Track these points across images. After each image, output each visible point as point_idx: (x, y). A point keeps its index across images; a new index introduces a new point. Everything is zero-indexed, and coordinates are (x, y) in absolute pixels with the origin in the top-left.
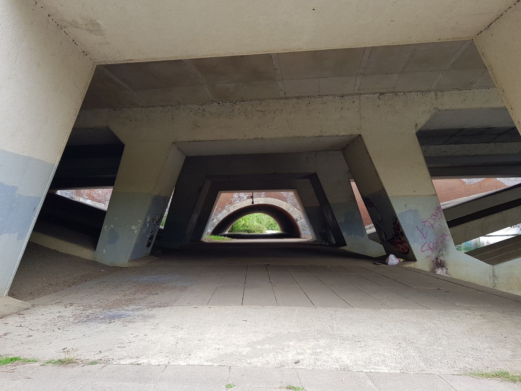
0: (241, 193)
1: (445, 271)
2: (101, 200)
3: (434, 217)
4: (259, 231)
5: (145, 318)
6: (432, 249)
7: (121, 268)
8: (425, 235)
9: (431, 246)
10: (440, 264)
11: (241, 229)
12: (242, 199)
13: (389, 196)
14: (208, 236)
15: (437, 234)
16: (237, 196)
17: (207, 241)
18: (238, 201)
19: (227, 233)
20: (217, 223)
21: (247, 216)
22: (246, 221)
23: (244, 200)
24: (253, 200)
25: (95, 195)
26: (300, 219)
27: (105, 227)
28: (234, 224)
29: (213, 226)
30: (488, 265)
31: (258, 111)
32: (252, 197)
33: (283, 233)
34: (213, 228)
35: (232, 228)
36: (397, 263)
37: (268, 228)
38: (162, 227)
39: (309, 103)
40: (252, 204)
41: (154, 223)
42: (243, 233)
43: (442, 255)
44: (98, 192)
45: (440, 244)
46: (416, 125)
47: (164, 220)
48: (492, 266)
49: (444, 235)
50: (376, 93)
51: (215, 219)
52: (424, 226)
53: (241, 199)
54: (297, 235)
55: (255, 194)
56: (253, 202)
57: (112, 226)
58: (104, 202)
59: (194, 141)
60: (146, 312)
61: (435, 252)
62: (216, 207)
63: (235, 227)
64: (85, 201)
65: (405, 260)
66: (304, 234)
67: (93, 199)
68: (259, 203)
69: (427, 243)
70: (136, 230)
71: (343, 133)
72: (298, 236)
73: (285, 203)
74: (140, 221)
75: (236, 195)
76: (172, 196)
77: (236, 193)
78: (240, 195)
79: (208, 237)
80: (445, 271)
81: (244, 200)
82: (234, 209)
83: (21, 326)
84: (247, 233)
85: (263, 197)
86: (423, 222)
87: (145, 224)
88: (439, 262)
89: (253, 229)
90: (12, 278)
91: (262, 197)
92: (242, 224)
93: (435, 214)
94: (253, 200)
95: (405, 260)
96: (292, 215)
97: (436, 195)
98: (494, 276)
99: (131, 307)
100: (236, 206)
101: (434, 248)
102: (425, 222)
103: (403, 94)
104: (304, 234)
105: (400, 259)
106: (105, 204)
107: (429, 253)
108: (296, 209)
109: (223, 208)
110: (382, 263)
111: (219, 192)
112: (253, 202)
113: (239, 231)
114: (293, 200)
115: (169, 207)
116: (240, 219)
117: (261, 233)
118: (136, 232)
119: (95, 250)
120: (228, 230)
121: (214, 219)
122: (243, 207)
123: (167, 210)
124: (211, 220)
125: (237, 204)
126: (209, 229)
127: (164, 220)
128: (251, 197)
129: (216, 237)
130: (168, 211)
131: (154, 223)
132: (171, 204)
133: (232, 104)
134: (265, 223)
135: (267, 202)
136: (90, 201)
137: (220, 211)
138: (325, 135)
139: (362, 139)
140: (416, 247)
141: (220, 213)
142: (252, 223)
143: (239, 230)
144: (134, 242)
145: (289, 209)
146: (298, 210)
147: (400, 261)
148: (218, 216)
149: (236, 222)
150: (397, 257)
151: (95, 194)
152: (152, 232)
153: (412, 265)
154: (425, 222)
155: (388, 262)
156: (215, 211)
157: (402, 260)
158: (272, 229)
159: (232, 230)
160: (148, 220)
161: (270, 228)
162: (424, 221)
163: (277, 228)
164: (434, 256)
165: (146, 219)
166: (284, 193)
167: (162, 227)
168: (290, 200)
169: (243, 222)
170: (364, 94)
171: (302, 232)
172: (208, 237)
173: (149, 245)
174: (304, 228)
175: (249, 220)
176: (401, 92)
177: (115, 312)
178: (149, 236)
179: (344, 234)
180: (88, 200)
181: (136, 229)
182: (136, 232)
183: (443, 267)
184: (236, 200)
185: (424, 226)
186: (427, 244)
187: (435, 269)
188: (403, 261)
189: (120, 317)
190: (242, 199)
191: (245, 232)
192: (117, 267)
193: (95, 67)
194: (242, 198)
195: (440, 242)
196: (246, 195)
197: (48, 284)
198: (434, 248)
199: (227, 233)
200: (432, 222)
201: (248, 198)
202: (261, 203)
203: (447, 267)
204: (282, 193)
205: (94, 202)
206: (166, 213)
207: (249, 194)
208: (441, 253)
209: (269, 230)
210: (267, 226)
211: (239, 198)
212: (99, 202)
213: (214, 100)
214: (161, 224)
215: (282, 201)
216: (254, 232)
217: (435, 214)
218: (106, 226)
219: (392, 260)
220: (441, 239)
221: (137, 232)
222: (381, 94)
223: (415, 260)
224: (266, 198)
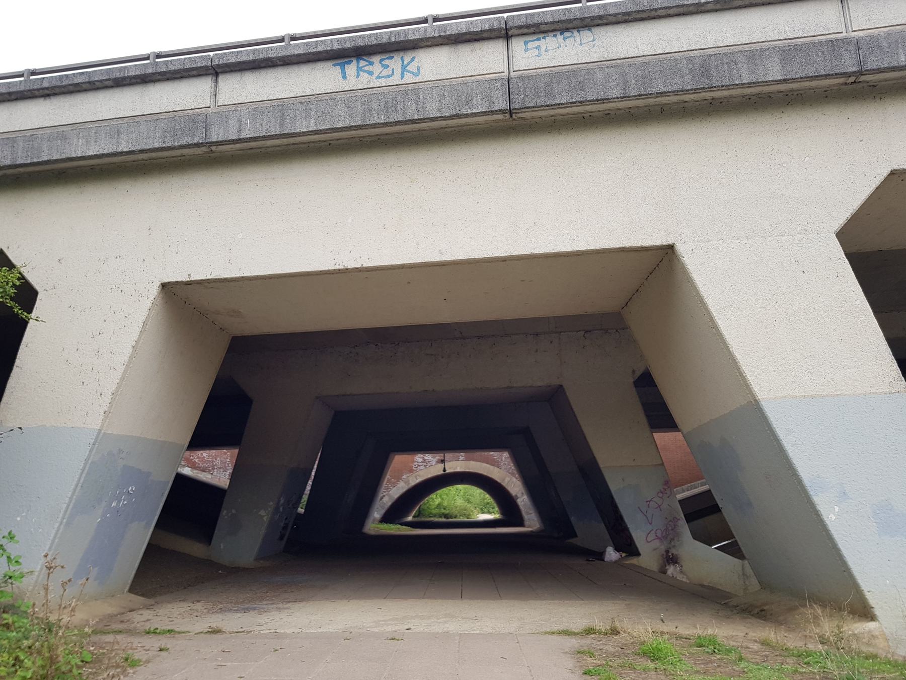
0: (427, 455)
1: (679, 568)
2: (207, 467)
3: (660, 495)
5: (279, 609)
6: (660, 538)
7: (245, 570)
8: (650, 521)
9: (659, 535)
10: (671, 559)
11: (434, 512)
12: (429, 464)
13: (601, 466)
14: (374, 525)
15: (666, 518)
16: (421, 460)
17: (372, 533)
18: (422, 467)
19: (410, 518)
20: (390, 504)
21: (445, 489)
22: (442, 499)
24: (444, 466)
25: (197, 461)
27: (224, 513)
28: (421, 503)
30: (736, 560)
31: (427, 354)
32: (443, 461)
33: (405, 518)
34: (383, 512)
36: (617, 559)
37: (482, 509)
38: (301, 510)
39: (494, 344)
40: (443, 472)
41: (291, 505)
42: (436, 519)
43: (674, 546)
44: (202, 454)
45: (671, 532)
46: (634, 371)
47: (305, 498)
48: (741, 561)
49: (675, 520)
50: (580, 331)
51: (386, 497)
52: (649, 507)
54: (520, 522)
55: (448, 456)
56: (444, 468)
57: (234, 511)
58: (210, 471)
59: (343, 395)
60: (280, 606)
61: (665, 542)
62: (388, 477)
64: (182, 470)
65: (627, 554)
67: (193, 466)
69: (653, 530)
70: (266, 516)
71: (539, 384)
72: (520, 522)
73: (496, 469)
74: (271, 503)
75: (419, 458)
76: (318, 459)
77: (419, 455)
78: (426, 458)
79: (374, 525)
80: (679, 568)
81: (432, 465)
82: (417, 479)
83: (157, 615)
84: (444, 520)
86: (647, 501)
87: (277, 509)
88: (671, 556)
89: (456, 512)
90: (134, 572)
91: (461, 460)
92: (437, 503)
93: (662, 490)
94: (444, 466)
95: (627, 554)
96: (509, 489)
97: (663, 464)
98: (744, 574)
99: (265, 602)
101: (663, 537)
102: (650, 501)
103: (615, 331)
105: (621, 553)
106: (212, 474)
107: (657, 543)
109: (399, 478)
110: (598, 559)
111: (391, 455)
112: (444, 468)
113: (431, 515)
114: (509, 465)
115: (313, 477)
116: (433, 496)
118: (265, 518)
119: (210, 544)
121: (384, 496)
122: (430, 476)
123: (310, 482)
124: (379, 498)
125: (421, 473)
126: (377, 514)
127: (305, 498)
129: (392, 526)
130: (311, 483)
131: (291, 505)
132: (316, 472)
133: (393, 345)
134: (478, 501)
136: (190, 469)
137: (394, 483)
138: (515, 385)
139: (564, 390)
140: (639, 536)
141: (394, 487)
142: (453, 502)
143: (431, 513)
144: (263, 532)
145: (504, 480)
147: (621, 556)
148: (390, 492)
150: (617, 549)
151: (198, 458)
152: (286, 519)
153: (634, 561)
154: (650, 501)
155: (604, 558)
156: (385, 483)
157: (624, 555)
158: (489, 513)
159: (419, 514)
160: (282, 501)
162: (648, 500)
164: (663, 548)
165: (279, 501)
166: (495, 455)
167: (301, 510)
168: (505, 464)
169: (438, 501)
170: (564, 332)
171: (526, 517)
172: (374, 525)
173: (281, 538)
175: (448, 496)
176: (612, 329)
177: (247, 606)
178: (282, 524)
179: (573, 519)
180: (187, 468)
181: (265, 515)
182: (265, 518)
183: (676, 563)
185: (649, 507)
186: (653, 532)
187: (666, 566)
188: (626, 556)
189: (254, 609)
190: (429, 464)
191: (441, 517)
192: (239, 568)
193: (231, 338)
194: (429, 462)
195: (670, 528)
196: (434, 457)
197: (159, 586)
198: (663, 537)
199: (410, 518)
200: (659, 501)
201: (438, 462)
202: (458, 470)
203: (681, 563)
204: (492, 453)
205: (195, 471)
206: (309, 488)
207: (439, 456)
208: (673, 543)
209: (483, 513)
210: (481, 507)
212: (204, 471)
213: (369, 341)
214: (301, 505)
215: (492, 467)
216: (456, 517)
217: (662, 490)
218: (225, 512)
219: (610, 554)
220: (672, 524)
221: (267, 519)
222: (586, 332)
223: (638, 554)
224: (468, 463)
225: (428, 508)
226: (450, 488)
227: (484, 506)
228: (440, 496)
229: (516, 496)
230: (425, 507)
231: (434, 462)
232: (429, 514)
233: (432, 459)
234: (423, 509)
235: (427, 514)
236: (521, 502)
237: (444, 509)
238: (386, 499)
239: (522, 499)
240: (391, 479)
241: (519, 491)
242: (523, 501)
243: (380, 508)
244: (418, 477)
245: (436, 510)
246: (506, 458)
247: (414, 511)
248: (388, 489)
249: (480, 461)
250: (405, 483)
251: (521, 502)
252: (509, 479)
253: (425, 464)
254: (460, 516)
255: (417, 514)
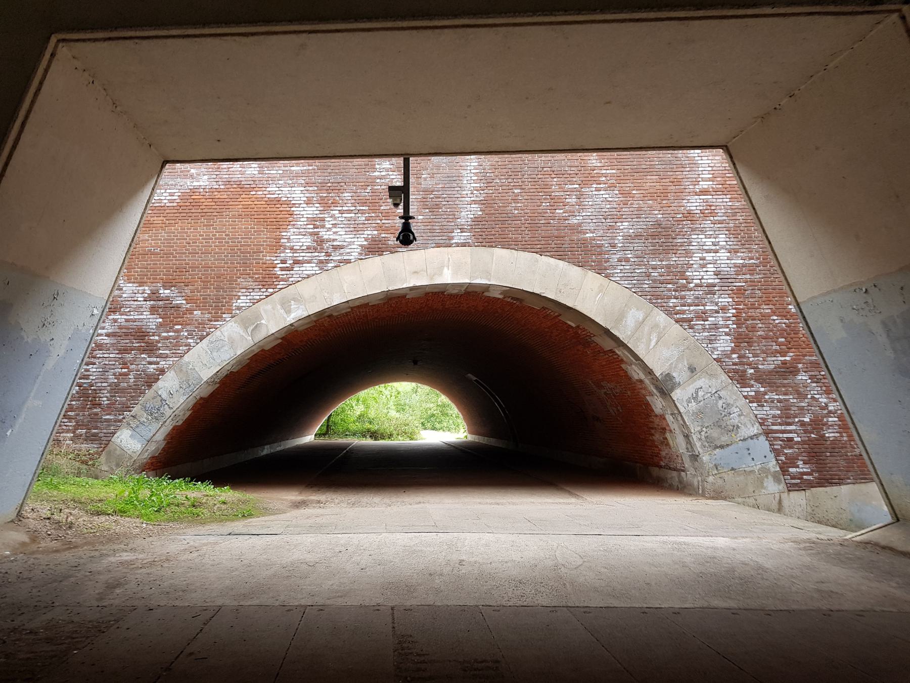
4: (406, 433)
11: (353, 427)
16: (307, 241)
18: (309, 268)
23: (348, 262)
26: (686, 374)
29: (154, 414)
33: (289, 441)
35: (328, 426)
37: (423, 424)
53: (328, 254)
63: (336, 421)
66: (716, 467)
68: (439, 281)
73: (592, 280)
82: (288, 312)
84: (368, 442)
85: (464, 245)
89: (387, 427)
91: (458, 245)
92: (358, 413)
100: (298, 299)
104: (716, 467)
108: (661, 318)
113: (347, 433)
117: (412, 439)
120: (316, 429)
121: (162, 372)
122: (337, 299)
125: (305, 288)
128: (392, 189)
135: (488, 274)
137: (201, 325)
143: (348, 429)
145: (622, 316)
146: (677, 322)
148: (186, 358)
149: (341, 405)
161: (429, 425)
163: (445, 424)
169: (359, 409)
174: (715, 433)
175: (377, 402)
184: (296, 262)
191: (364, 436)
194: (335, 248)
202: (447, 277)
209: (425, 429)
211: (315, 249)
215: (575, 272)
224: (484, 253)
225: (342, 420)
226: (381, 388)
227: (426, 419)
228: (364, 402)
229: (669, 377)
230: (338, 419)
231: (354, 252)
232: (344, 432)
233: (348, 238)
234: (335, 424)
235: (341, 431)
236: (689, 402)
237: (370, 423)
238: (168, 384)
239: (690, 389)
240: (190, 311)
241: (680, 359)
242: (695, 398)
243: (144, 417)
244: (293, 305)
245: (357, 424)
246: (627, 237)
247: (317, 426)
248: (177, 345)
249: (525, 247)
250: (245, 324)
251: (689, 402)
252: (640, 315)
253: (322, 257)
254: (398, 435)
255: (324, 431)
